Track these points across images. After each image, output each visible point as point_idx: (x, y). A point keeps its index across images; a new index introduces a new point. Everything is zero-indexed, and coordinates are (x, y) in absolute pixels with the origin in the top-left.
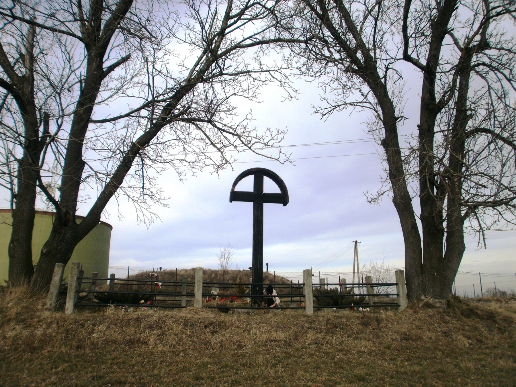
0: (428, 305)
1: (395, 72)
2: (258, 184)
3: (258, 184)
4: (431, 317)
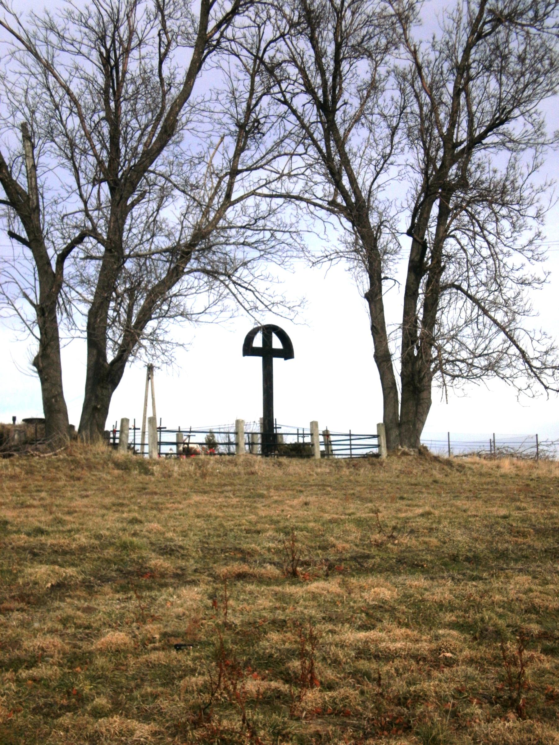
0: (405, 454)
1: (272, 45)
2: (267, 340)
3: (267, 340)
4: (411, 461)
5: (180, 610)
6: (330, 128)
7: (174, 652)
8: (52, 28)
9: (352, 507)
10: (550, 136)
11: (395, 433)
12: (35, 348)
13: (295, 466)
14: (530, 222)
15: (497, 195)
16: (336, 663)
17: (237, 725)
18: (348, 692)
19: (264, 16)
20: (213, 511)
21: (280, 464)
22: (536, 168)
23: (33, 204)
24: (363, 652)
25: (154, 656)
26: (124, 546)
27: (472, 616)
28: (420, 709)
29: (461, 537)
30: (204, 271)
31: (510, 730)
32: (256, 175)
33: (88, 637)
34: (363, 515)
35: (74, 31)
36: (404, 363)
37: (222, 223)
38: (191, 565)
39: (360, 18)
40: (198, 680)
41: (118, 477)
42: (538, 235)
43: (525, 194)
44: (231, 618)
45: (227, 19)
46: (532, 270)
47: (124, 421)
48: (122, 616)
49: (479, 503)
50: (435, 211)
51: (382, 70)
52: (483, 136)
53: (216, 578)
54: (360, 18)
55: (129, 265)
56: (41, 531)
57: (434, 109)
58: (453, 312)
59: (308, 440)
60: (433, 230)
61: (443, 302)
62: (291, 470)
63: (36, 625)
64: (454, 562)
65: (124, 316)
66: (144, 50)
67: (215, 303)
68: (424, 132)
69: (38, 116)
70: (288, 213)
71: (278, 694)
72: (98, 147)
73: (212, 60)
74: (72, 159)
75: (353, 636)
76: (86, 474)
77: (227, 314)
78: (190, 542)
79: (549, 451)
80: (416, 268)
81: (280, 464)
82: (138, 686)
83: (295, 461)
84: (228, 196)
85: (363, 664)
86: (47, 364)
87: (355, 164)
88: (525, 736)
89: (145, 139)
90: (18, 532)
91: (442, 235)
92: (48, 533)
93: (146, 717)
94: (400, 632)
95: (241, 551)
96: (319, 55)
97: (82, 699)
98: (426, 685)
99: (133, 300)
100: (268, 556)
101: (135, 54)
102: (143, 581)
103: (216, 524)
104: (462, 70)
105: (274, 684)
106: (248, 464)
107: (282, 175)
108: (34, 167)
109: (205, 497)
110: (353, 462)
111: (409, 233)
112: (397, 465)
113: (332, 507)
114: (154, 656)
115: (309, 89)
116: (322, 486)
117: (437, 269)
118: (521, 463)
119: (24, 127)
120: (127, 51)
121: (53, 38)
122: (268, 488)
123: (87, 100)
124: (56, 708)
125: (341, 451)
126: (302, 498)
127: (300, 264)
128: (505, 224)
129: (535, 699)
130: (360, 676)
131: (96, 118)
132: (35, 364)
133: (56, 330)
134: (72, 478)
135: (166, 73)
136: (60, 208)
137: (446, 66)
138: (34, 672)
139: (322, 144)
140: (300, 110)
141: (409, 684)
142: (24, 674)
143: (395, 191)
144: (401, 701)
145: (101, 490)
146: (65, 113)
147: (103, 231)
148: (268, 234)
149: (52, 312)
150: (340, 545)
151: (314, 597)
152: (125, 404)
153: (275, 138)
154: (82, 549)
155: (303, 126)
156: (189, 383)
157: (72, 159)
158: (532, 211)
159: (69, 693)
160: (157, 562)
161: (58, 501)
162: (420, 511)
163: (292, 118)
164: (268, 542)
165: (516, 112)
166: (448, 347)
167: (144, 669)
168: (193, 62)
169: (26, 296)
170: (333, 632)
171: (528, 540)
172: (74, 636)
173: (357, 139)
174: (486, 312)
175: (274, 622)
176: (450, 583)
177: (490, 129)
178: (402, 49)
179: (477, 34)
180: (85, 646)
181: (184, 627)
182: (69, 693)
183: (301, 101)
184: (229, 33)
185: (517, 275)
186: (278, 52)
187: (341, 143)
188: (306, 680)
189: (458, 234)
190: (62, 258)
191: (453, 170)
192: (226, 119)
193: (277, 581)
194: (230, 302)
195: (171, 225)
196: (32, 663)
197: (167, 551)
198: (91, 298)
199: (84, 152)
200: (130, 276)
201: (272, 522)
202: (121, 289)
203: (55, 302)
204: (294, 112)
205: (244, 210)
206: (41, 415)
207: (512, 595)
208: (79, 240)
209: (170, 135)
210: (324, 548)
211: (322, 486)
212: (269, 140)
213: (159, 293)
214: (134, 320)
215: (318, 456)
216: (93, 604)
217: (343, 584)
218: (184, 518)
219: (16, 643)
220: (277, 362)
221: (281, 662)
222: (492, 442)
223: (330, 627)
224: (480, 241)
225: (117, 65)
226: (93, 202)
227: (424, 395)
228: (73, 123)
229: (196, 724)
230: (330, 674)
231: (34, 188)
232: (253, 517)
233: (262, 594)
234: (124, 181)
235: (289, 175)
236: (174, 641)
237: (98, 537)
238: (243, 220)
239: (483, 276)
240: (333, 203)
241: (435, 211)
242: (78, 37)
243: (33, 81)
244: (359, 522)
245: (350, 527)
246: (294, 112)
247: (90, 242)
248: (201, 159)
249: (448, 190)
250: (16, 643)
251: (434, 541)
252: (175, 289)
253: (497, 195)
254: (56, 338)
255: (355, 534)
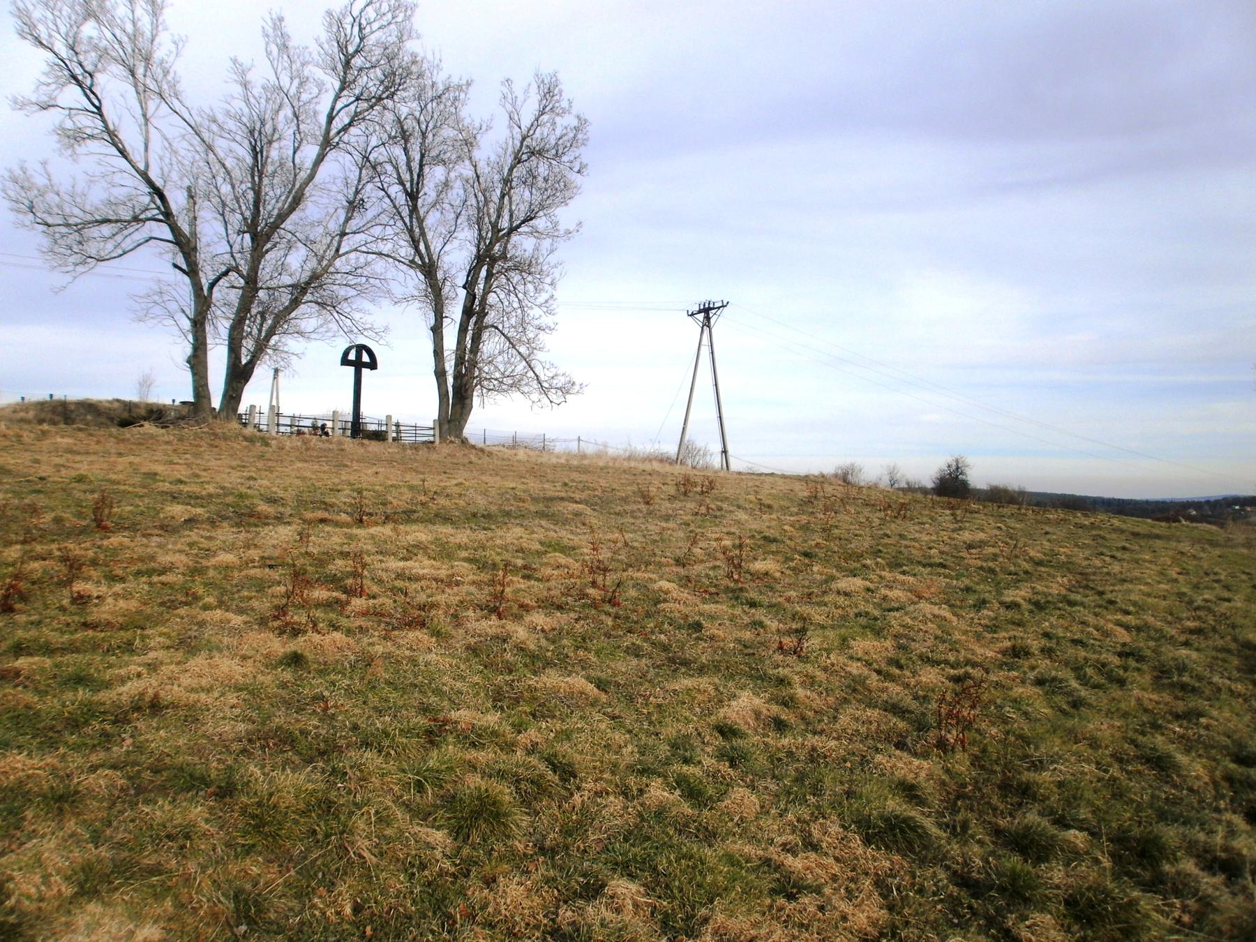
0: (452, 442)
2: (359, 355)
3: (359, 355)
5: (275, 542)
6: (414, 210)
7: (267, 570)
8: (215, 121)
9: (408, 477)
10: (562, 232)
11: (446, 427)
12: (189, 350)
13: (374, 446)
14: (547, 287)
15: (525, 267)
16: (381, 581)
17: (304, 620)
18: (386, 602)
19: (371, 129)
20: (308, 474)
21: (363, 444)
22: (552, 251)
23: (192, 245)
24: (400, 576)
25: (252, 572)
26: (241, 496)
27: (480, 553)
28: (433, 612)
29: (481, 502)
30: (317, 303)
31: (491, 627)
32: (360, 238)
33: (207, 557)
34: (416, 482)
35: (231, 125)
36: (455, 378)
37: (332, 269)
38: (288, 511)
39: (438, 139)
40: (282, 589)
41: (246, 447)
42: (552, 296)
43: (544, 268)
44: (310, 549)
45: (345, 129)
46: (546, 320)
47: (253, 407)
48: (233, 544)
49: (498, 478)
50: (483, 273)
51: (453, 175)
52: (519, 226)
53: (305, 521)
54: (438, 139)
55: (261, 294)
56: (181, 482)
57: (486, 202)
58: (491, 345)
59: (384, 428)
60: (481, 286)
61: (485, 336)
62: (370, 449)
63: (170, 546)
64: (475, 518)
65: (255, 331)
66: (283, 143)
67: (321, 326)
68: (479, 221)
69: (200, 182)
70: (379, 265)
71: (337, 601)
72: (244, 208)
73: (332, 155)
74: (223, 215)
75: (395, 564)
76: (223, 444)
77: (330, 334)
78: (289, 495)
79: (550, 445)
80: (468, 312)
81: (363, 444)
82: (238, 591)
83: (373, 443)
84: (337, 250)
85: (399, 584)
86: (197, 361)
87: (429, 236)
88: (499, 630)
89: (280, 205)
90: (164, 481)
91: (487, 291)
92: (185, 483)
93: (240, 611)
94: (427, 562)
95: (325, 503)
96: (409, 161)
97: (196, 598)
98: (439, 598)
99: (264, 319)
100: (343, 507)
101: (275, 145)
102: (252, 520)
103: (309, 483)
104: (507, 181)
105: (335, 594)
106: (340, 443)
108: (195, 218)
109: (306, 465)
110: (415, 446)
111: (464, 287)
112: (446, 449)
113: (393, 476)
114: (252, 572)
115: (401, 183)
116: (390, 462)
117: (483, 314)
118: (531, 453)
119: (189, 189)
120: (270, 142)
121: (214, 127)
122: (352, 461)
123: (237, 174)
124: (176, 603)
125: (407, 438)
126: (375, 469)
127: (386, 303)
128: (530, 287)
129: (511, 607)
130: (395, 591)
131: (243, 187)
132: (188, 362)
133: (205, 338)
134: (212, 446)
135: (297, 161)
136: (211, 249)
137: (497, 177)
138: (163, 578)
139: (407, 220)
140: (393, 196)
141: (429, 596)
142: (155, 579)
143: (457, 257)
144: (422, 607)
145: (231, 456)
146: (220, 180)
147: (244, 269)
148: (364, 279)
149: (203, 324)
150: (395, 502)
151: (373, 537)
152: (254, 396)
153: (375, 213)
154: (210, 496)
155: (395, 207)
156: (302, 384)
157: (223, 215)
158: (548, 280)
159: (187, 594)
160: (263, 507)
161: (199, 461)
162: (455, 482)
163: (387, 200)
164: (343, 498)
165: (541, 213)
166: (486, 369)
167: (245, 580)
168: (318, 156)
169: (183, 312)
170: (381, 561)
171: (526, 505)
172: (197, 555)
173: (431, 220)
174: (514, 347)
175: (341, 553)
176: (468, 531)
177: (523, 222)
178: (467, 162)
179: (518, 160)
180: (205, 563)
181: (277, 553)
182: (187, 594)
183: (395, 190)
184: (346, 138)
185: (536, 322)
186: (378, 155)
187: (421, 221)
188: (360, 592)
189: (498, 290)
190: (212, 285)
191: (497, 247)
192: (340, 197)
193: (348, 525)
194: (334, 326)
195: (293, 268)
196: (162, 572)
197: (272, 501)
198: (233, 316)
199: (233, 211)
200: (261, 303)
201: (350, 484)
202: (254, 311)
203: (205, 318)
204: (389, 196)
205: (347, 261)
206: (190, 398)
207: (509, 541)
208: (226, 274)
209: (298, 204)
210: (384, 504)
211: (390, 462)
212: (370, 214)
213: (282, 317)
214: (263, 334)
215: (390, 440)
216: (213, 534)
217: (395, 529)
218: (287, 479)
219: (152, 558)
220: (365, 371)
221: (342, 579)
222: (514, 438)
223: (380, 557)
224: (513, 297)
225: (262, 152)
226: (236, 247)
227: (468, 401)
228: (226, 189)
229: (276, 618)
230: (375, 589)
231: (194, 234)
232: (336, 481)
233: (336, 533)
234: (261, 234)
235: (382, 239)
236: (269, 562)
237: (223, 488)
238: (348, 269)
239: (513, 321)
240: (412, 261)
241: (483, 273)
242: (234, 129)
243: (197, 157)
244: (411, 488)
245: (405, 490)
246: (389, 196)
247: (233, 276)
248: (320, 223)
249: (494, 260)
250: (152, 558)
251: (462, 503)
252: (293, 315)
253: (525, 267)
254: (205, 344)
255: (408, 495)
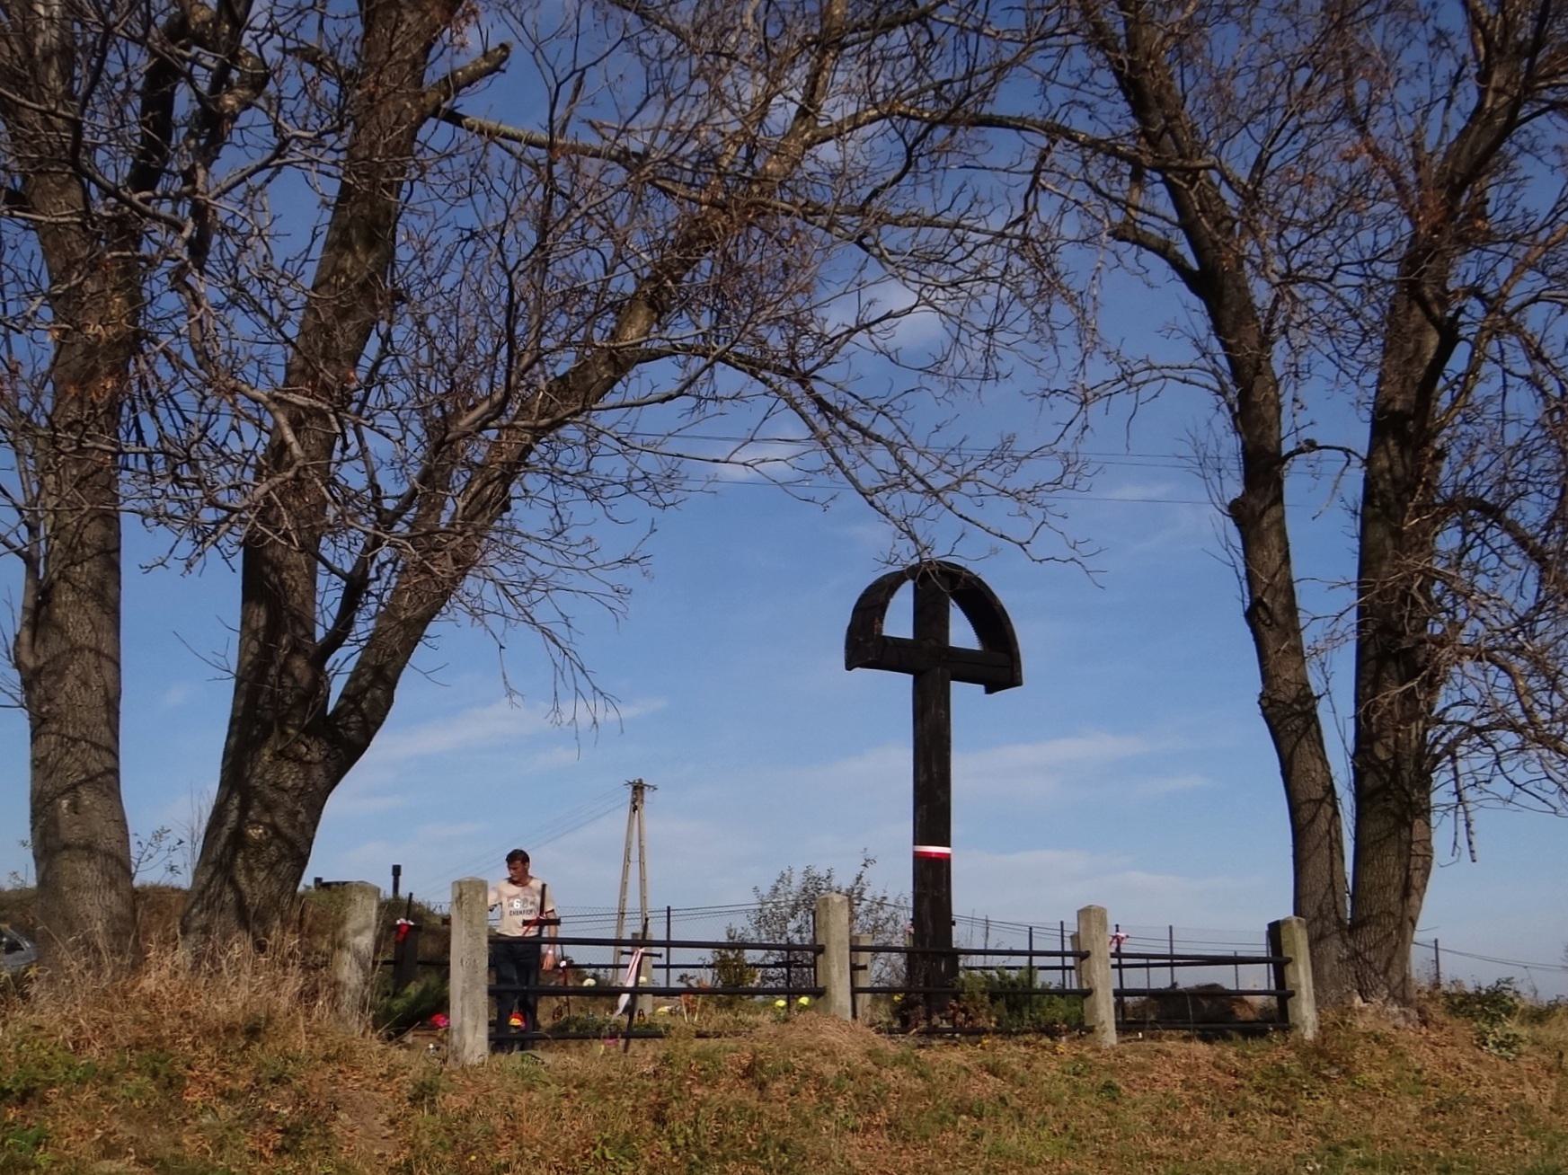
2: (929, 617)
107: (1505, 371)
152: (368, 834)
220: (965, 697)
